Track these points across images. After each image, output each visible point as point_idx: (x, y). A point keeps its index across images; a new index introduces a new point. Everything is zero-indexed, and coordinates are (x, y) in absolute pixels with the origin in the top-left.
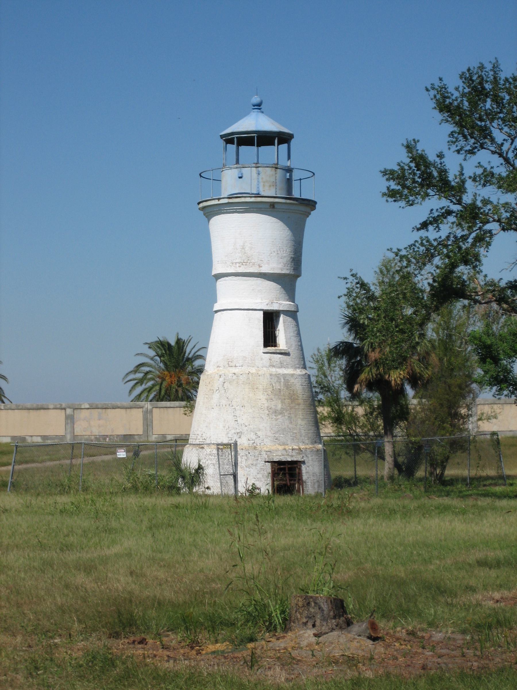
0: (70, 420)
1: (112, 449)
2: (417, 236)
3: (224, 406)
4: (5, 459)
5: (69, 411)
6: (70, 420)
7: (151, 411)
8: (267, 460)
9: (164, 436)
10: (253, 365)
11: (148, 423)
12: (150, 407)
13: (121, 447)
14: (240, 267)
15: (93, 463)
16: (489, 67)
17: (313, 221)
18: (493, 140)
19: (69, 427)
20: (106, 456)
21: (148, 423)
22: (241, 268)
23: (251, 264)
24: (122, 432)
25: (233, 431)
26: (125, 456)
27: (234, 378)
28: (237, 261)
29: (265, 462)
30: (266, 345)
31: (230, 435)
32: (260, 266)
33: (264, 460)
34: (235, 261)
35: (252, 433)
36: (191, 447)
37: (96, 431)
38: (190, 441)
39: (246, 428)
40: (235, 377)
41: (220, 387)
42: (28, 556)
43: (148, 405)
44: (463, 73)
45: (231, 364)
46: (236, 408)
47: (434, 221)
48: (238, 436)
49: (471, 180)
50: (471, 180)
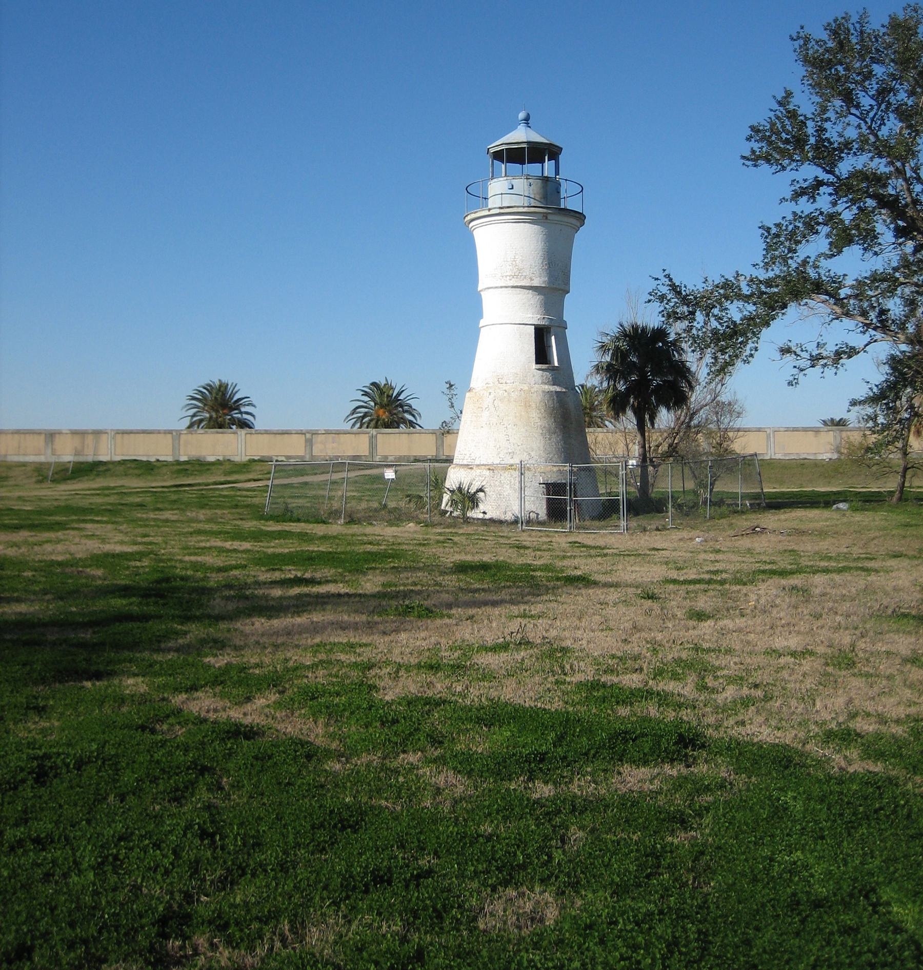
0: (309, 443)
2: (789, 208)
5: (308, 436)
6: (309, 443)
7: (376, 436)
9: (386, 457)
11: (373, 446)
12: (375, 433)
13: (783, 494)
16: (854, 19)
17: (581, 239)
18: (858, 106)
19: (308, 448)
21: (373, 446)
24: (351, 453)
30: (538, 361)
31: (501, 455)
32: (532, 280)
36: (457, 469)
37: (330, 453)
38: (455, 462)
40: (506, 394)
42: (301, 880)
43: (374, 431)
44: (829, 24)
47: (810, 191)
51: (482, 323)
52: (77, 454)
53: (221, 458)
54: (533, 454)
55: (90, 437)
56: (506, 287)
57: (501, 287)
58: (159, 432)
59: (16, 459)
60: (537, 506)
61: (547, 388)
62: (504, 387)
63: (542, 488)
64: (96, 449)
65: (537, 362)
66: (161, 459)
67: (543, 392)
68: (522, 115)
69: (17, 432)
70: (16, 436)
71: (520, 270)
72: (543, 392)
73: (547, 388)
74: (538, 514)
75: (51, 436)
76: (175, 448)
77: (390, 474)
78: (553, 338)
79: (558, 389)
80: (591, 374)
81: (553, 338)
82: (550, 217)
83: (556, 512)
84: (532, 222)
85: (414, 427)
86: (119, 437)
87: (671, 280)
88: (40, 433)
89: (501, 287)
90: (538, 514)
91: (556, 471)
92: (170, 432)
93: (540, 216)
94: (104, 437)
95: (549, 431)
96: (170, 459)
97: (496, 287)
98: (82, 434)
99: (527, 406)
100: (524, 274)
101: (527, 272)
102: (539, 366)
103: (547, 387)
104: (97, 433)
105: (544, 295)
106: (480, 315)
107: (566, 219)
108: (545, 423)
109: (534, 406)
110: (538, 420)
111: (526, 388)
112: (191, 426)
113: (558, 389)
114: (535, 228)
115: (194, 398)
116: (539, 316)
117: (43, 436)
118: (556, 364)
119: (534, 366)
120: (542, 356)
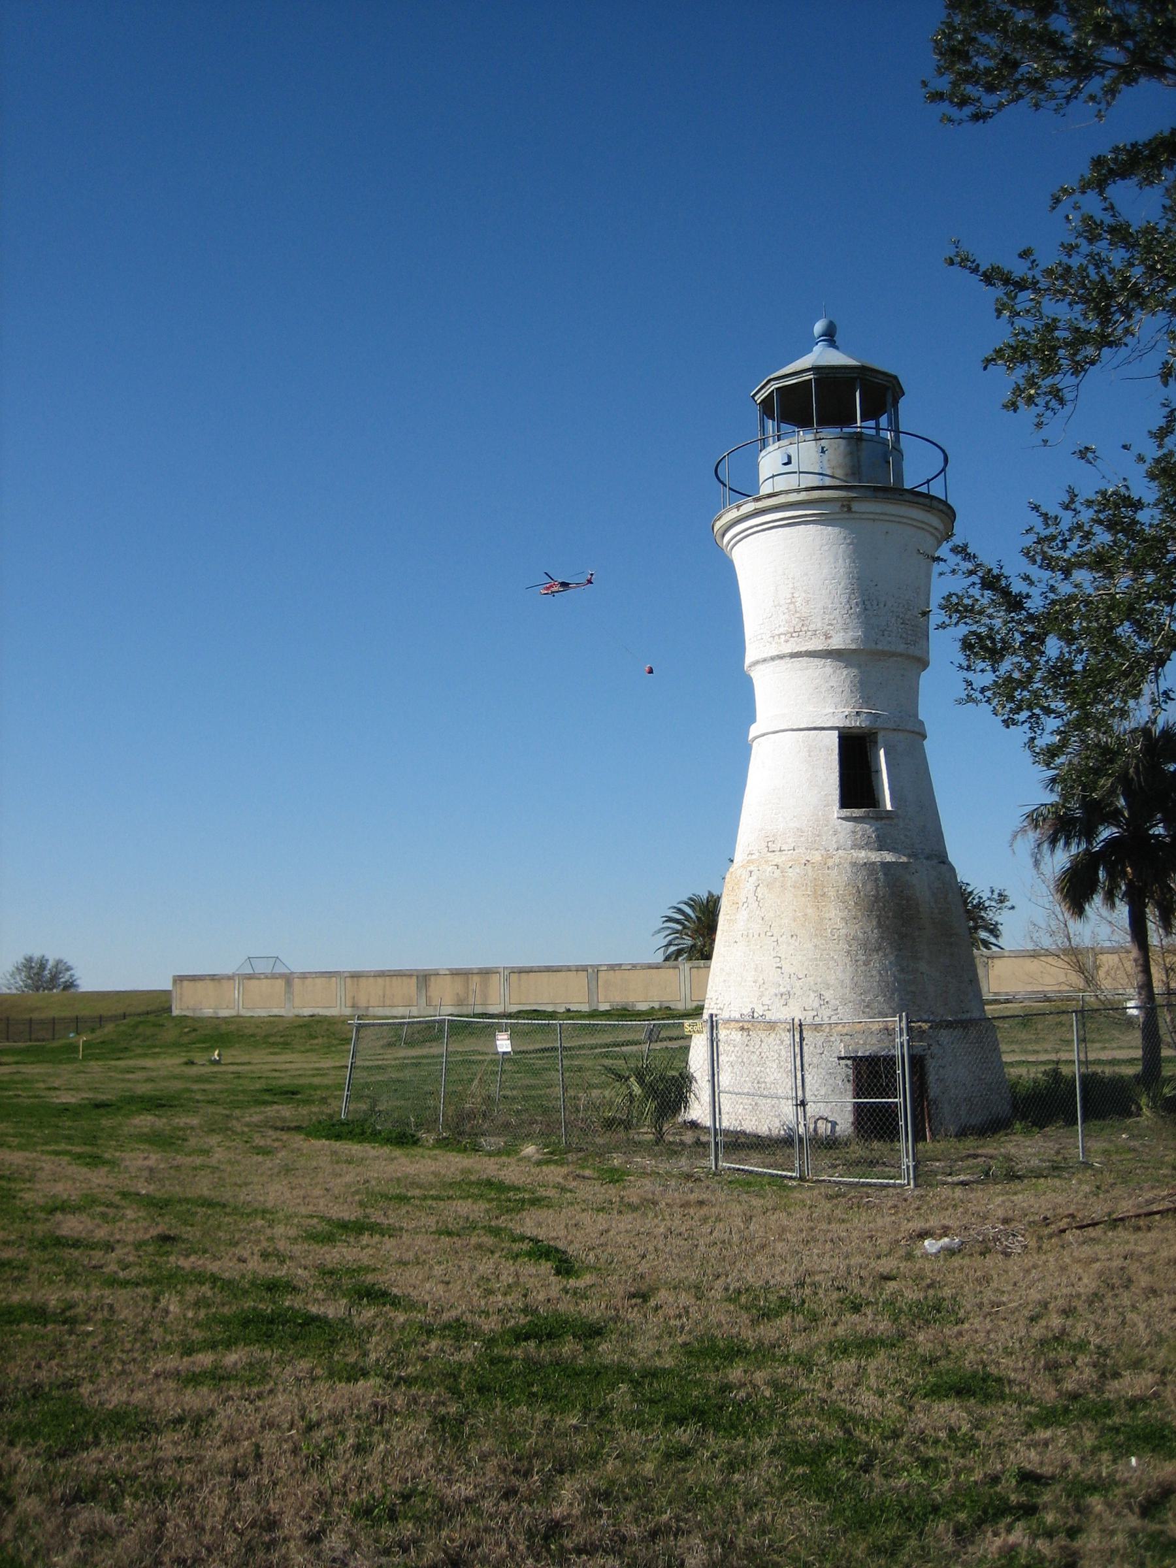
1: (489, 1032)
3: (756, 936)
4: (5, 1059)
8: (843, 1055)
10: (816, 846)
14: (787, 641)
15: (43, 1047)
20: (675, 1042)
22: (789, 644)
23: (809, 633)
25: (774, 991)
26: (509, 1049)
27: (775, 875)
28: (782, 630)
29: (840, 1058)
32: (827, 637)
33: (836, 1055)
34: (777, 632)
35: (812, 995)
39: (798, 984)
41: (751, 895)
45: (772, 846)
46: (780, 940)
48: (783, 1002)
49: (1024, 593)
50: (1024, 593)
51: (754, 731)
52: (460, 1003)
53: (657, 1006)
54: (828, 995)
55: (476, 979)
56: (781, 657)
57: (773, 659)
58: (568, 969)
59: (380, 1012)
60: (833, 1105)
61: (862, 855)
62: (778, 859)
63: (845, 1070)
64: (485, 996)
65: (845, 803)
66: (573, 1008)
67: (854, 864)
68: (819, 327)
69: (381, 974)
70: (380, 980)
71: (802, 620)
72: (854, 864)
73: (862, 855)
74: (834, 1124)
75: (424, 978)
76: (592, 990)
77: (504, 1044)
78: (882, 752)
79: (889, 857)
80: (1023, 830)
81: (882, 752)
82: (855, 506)
83: (874, 1123)
84: (821, 520)
85: (989, 949)
86: (514, 977)
87: (968, 557)
88: (411, 976)
89: (773, 659)
90: (834, 1124)
91: (890, 1033)
92: (584, 969)
93: (836, 507)
94: (495, 978)
95: (864, 945)
96: (585, 1008)
97: (765, 660)
98: (461, 974)
99: (818, 895)
100: (812, 627)
101: (817, 623)
102: (847, 812)
103: (863, 854)
104: (486, 973)
105: (859, 667)
106: (750, 716)
107: (891, 508)
108: (855, 929)
109: (832, 893)
110: (841, 925)
111: (817, 857)
112: (667, 959)
113: (889, 857)
114: (830, 531)
115: (670, 919)
116: (847, 711)
117: (414, 979)
118: (889, 807)
119: (835, 810)
120: (856, 787)
